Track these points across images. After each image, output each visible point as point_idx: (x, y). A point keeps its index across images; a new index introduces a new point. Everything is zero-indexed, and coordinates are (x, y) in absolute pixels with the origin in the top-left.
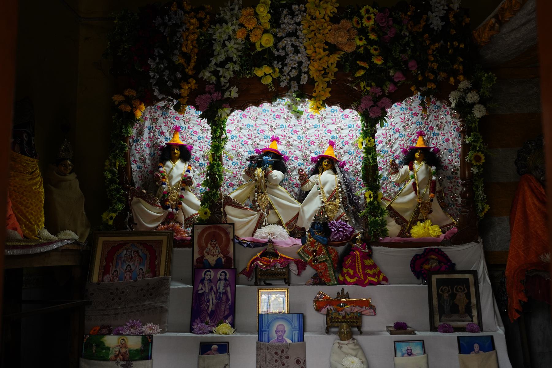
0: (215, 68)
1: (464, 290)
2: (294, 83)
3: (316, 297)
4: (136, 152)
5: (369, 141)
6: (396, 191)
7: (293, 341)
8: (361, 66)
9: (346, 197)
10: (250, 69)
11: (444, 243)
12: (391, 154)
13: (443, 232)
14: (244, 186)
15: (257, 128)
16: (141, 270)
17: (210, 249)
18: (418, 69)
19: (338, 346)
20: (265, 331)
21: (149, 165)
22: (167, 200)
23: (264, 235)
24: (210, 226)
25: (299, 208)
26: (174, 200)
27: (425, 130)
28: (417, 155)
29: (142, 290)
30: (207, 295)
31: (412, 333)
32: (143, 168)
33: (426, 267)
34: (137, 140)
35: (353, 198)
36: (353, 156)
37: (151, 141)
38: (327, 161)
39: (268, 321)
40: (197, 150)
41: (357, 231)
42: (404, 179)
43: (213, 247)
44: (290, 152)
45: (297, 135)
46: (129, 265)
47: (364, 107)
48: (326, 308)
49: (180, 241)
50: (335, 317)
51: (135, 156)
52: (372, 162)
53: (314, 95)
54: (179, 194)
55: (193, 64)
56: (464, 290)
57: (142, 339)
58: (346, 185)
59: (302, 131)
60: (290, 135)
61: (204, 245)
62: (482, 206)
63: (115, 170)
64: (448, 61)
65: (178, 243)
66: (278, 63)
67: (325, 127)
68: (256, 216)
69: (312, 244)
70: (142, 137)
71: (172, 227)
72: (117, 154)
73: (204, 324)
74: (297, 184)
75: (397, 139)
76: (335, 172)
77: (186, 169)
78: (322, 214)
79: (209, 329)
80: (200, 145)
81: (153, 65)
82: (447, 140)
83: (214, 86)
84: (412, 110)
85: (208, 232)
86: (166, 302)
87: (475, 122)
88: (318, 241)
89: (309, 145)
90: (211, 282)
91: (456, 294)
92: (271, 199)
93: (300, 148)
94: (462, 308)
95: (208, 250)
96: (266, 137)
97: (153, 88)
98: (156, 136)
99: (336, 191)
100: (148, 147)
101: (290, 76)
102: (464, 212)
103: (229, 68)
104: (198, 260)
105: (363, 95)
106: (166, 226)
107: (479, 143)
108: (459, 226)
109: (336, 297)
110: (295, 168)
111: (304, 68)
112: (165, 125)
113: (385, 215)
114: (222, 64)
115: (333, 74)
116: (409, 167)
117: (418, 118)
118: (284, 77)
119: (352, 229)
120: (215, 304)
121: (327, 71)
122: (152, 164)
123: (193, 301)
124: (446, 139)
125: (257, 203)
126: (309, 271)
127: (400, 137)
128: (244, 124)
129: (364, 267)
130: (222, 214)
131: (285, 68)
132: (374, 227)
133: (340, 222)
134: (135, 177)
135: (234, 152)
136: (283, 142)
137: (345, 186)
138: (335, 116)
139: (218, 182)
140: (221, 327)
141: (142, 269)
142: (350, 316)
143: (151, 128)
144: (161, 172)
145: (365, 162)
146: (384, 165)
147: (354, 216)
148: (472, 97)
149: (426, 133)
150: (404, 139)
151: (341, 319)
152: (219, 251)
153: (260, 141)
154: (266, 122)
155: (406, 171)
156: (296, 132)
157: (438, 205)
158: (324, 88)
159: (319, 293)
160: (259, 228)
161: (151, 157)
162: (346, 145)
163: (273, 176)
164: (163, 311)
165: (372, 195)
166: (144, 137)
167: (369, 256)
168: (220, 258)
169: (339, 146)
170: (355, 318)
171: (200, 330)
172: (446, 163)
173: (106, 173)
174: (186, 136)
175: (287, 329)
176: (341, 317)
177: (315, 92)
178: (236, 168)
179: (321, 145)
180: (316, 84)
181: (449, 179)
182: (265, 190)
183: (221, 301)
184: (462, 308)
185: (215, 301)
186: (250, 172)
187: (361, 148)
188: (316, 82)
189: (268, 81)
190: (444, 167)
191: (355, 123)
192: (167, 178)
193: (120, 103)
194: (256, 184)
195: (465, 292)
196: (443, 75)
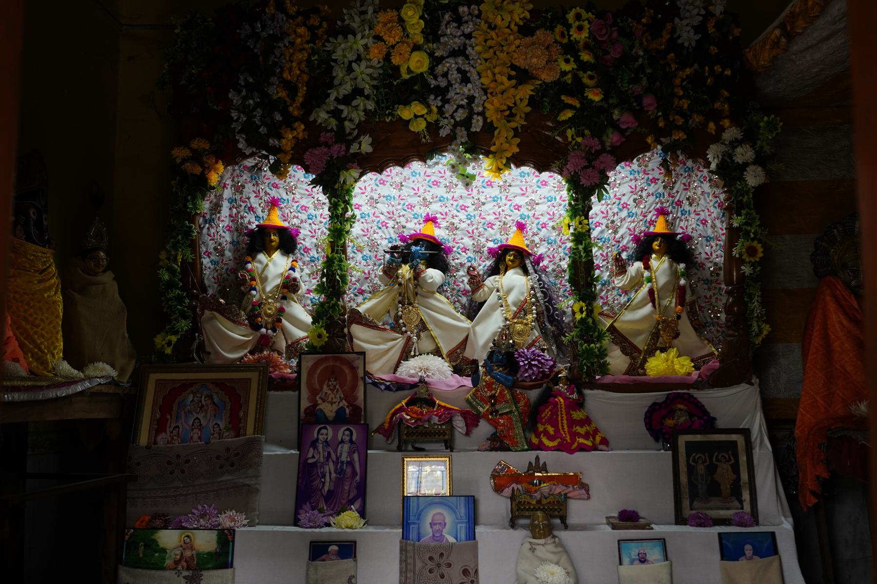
0: (335, 105)
4: (210, 238)
6: (622, 302)
9: (543, 311)
10: (391, 107)
11: (697, 385)
12: (614, 243)
13: (697, 368)
14: (382, 293)
15: (402, 202)
16: (216, 426)
17: (326, 393)
19: (530, 547)
20: (414, 523)
21: (230, 260)
22: (259, 315)
23: (412, 372)
24: (326, 357)
25: (469, 329)
26: (269, 316)
27: (669, 206)
28: (656, 245)
29: (218, 457)
33: (670, 422)
34: (210, 220)
35: (553, 312)
36: (555, 247)
37: (232, 221)
38: (513, 254)
39: (418, 508)
41: (560, 366)
42: (636, 283)
43: (330, 389)
44: (454, 239)
45: (466, 213)
46: (197, 418)
48: (511, 488)
50: (525, 501)
51: (208, 245)
52: (585, 256)
53: (493, 149)
54: (278, 305)
58: (542, 292)
59: (474, 207)
60: (455, 212)
61: (318, 387)
62: (759, 326)
63: (176, 266)
64: (706, 96)
65: (275, 383)
66: (435, 99)
67: (510, 200)
68: (400, 341)
69: (489, 386)
70: (218, 215)
71: (266, 358)
72: (178, 242)
73: (316, 512)
74: (464, 290)
75: (624, 219)
76: (526, 272)
77: (289, 266)
78: (504, 338)
80: (312, 228)
82: (704, 222)
84: (648, 174)
85: (324, 366)
86: (256, 476)
88: (498, 380)
89: (485, 229)
90: (329, 445)
91: (717, 466)
92: (424, 313)
93: (469, 233)
94: (726, 488)
95: (324, 394)
96: (416, 216)
97: (237, 138)
98: (242, 213)
99: (526, 302)
100: (229, 230)
101: (455, 119)
102: (730, 336)
103: (358, 106)
104: (308, 411)
105: (571, 150)
106: (256, 356)
107: (754, 226)
110: (462, 265)
111: (478, 106)
112: (256, 197)
113: (604, 340)
114: (347, 100)
115: (523, 116)
116: (643, 264)
117: (657, 186)
118: (446, 121)
121: (514, 111)
122: (235, 258)
123: (300, 475)
124: (702, 221)
125: (401, 321)
126: (484, 429)
127: (629, 216)
128: (382, 195)
129: (572, 422)
130: (347, 338)
131: (447, 106)
132: (587, 359)
133: (534, 351)
134: (207, 279)
135: (366, 238)
139: (340, 286)
140: (343, 516)
142: (548, 500)
143: (232, 200)
144: (248, 271)
146: (604, 260)
148: (743, 154)
149: (669, 210)
150: (636, 219)
152: (340, 397)
153: (407, 221)
154: (417, 192)
155: (638, 270)
156: (464, 208)
158: (509, 138)
159: (499, 464)
160: (404, 360)
163: (428, 277)
164: (252, 491)
165: (584, 309)
166: (222, 215)
167: (579, 404)
168: (342, 407)
169: (532, 231)
171: (309, 521)
172: (701, 258)
173: (160, 272)
174: (289, 214)
178: (369, 265)
179: (504, 228)
182: (415, 300)
183: (344, 476)
184: (726, 488)
185: (334, 475)
186: (390, 271)
187: (568, 233)
188: (496, 128)
189: (419, 126)
190: (699, 264)
192: (258, 280)
193: (184, 161)
194: (400, 290)
196: (697, 119)
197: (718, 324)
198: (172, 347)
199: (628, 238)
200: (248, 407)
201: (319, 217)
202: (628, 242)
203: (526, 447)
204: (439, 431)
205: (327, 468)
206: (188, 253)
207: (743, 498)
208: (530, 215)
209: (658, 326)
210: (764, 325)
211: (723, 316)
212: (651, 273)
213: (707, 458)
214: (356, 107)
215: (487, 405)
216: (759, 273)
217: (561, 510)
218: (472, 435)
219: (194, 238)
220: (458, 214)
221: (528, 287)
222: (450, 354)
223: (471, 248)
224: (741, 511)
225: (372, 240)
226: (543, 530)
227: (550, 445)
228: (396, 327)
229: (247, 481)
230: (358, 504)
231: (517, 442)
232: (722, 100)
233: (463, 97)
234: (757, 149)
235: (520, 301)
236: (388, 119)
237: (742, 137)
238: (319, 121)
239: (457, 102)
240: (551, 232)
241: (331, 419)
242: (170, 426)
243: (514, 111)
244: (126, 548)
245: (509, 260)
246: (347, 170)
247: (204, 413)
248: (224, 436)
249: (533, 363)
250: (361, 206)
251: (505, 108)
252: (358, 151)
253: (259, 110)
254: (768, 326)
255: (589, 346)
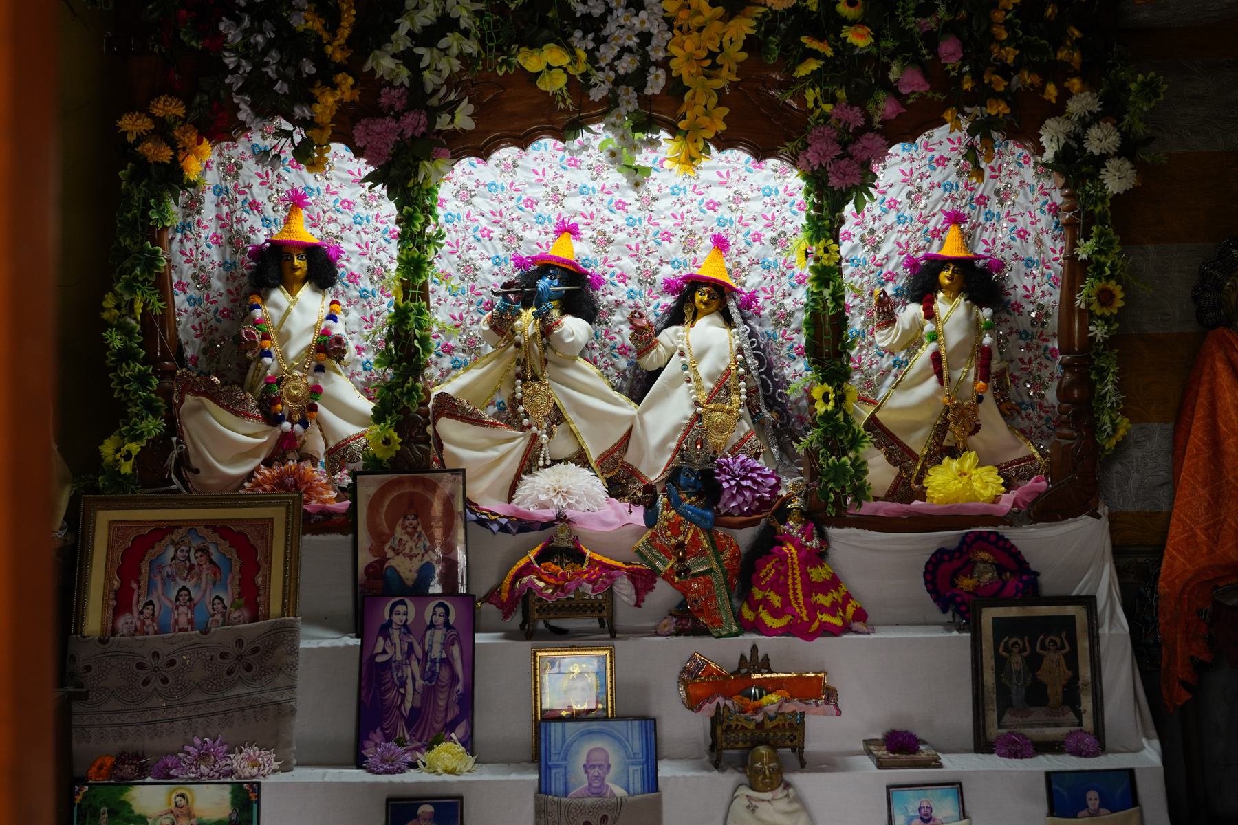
0: (409, 44)
1: (1063, 647)
2: (627, 90)
3: (685, 668)
4: (185, 258)
5: (826, 250)
6: (885, 366)
7: (631, 790)
8: (811, 49)
9: (757, 386)
10: (505, 48)
11: (1010, 519)
12: (873, 267)
13: (1008, 485)
14: (486, 360)
15: (516, 195)
16: (217, 601)
17: (401, 540)
18: (964, 61)
19: (748, 803)
20: (558, 766)
21: (221, 295)
22: (278, 400)
23: (543, 497)
24: (398, 479)
25: (633, 417)
26: (295, 400)
27: (966, 205)
28: (944, 277)
29: (223, 656)
30: (398, 669)
31: (933, 763)
32: (205, 304)
33: (966, 583)
34: (184, 226)
35: (774, 391)
36: (775, 274)
37: (222, 227)
38: (708, 292)
39: (564, 741)
40: (351, 252)
41: (788, 482)
42: (911, 343)
43: (408, 533)
44: (606, 260)
45: (626, 216)
46: (184, 588)
47: (815, 164)
48: (715, 703)
49: (321, 517)
50: (737, 725)
51: (181, 272)
52: (834, 308)
53: (681, 125)
54: (310, 380)
55: (345, 32)
56: (1063, 647)
57: (233, 792)
58: (756, 356)
59: (638, 204)
60: (607, 213)
61: (386, 530)
62: (1112, 421)
63: (133, 322)
64: (1044, 41)
65: (312, 521)
66: (584, 37)
67: (701, 193)
68: (520, 443)
69: (674, 527)
70: (197, 217)
71: (293, 474)
72: (136, 279)
73: (392, 745)
74: (623, 346)
75: (892, 227)
76: (728, 321)
77: (326, 312)
78: (699, 447)
79: (409, 758)
80: (361, 239)
81: (235, 36)
82: (1023, 234)
83: (403, 90)
84: (932, 150)
85: (395, 494)
86: (291, 687)
87: (1102, 200)
88: (688, 518)
89: (658, 243)
90: (409, 632)
91: (1042, 657)
92: (559, 393)
93: (631, 249)
94: (1055, 692)
95: (396, 542)
96: (541, 219)
97: (236, 101)
98: (238, 214)
99: (730, 373)
100: (216, 243)
101: (616, 72)
102: (1066, 437)
103: (448, 48)
104: (371, 570)
105: (812, 124)
106: (276, 470)
107: (1111, 255)
108: (1054, 471)
109: (735, 668)
110: (618, 304)
111: (656, 49)
112: (262, 184)
113: (863, 447)
114: (430, 36)
115: (734, 67)
116: (924, 310)
117: (947, 171)
118: (601, 75)
119: (773, 481)
120: (420, 690)
121: (719, 60)
122: (229, 291)
123: (363, 684)
124: (1019, 232)
125: (521, 409)
126: (663, 594)
127: (899, 222)
128: (482, 181)
129: (811, 588)
130: (431, 442)
131: (602, 48)
132: (834, 480)
133: (743, 462)
134: (183, 330)
135: (454, 258)
136: (586, 233)
138: (728, 162)
139: (419, 357)
140: (439, 753)
141: (221, 599)
142: (775, 722)
143: (221, 190)
144: (256, 323)
145: (812, 304)
146: (856, 297)
147: (778, 443)
148: (1100, 139)
149: (966, 213)
150: (910, 228)
151: (751, 730)
152: (424, 546)
153: (525, 228)
154: (541, 177)
155: (914, 319)
156: (622, 206)
157: (995, 409)
158: (710, 107)
159: (692, 658)
160: (525, 474)
161: (224, 272)
162: (757, 243)
163: (565, 334)
164: (284, 712)
165: (831, 396)
166: (204, 216)
167: (819, 556)
168: (428, 563)
169: (737, 246)
170: (787, 727)
171: (384, 761)
172: (1016, 296)
173: (107, 335)
174: (321, 214)
175: (614, 760)
176: (752, 726)
177: (684, 117)
178: (461, 304)
179: (690, 244)
180: (688, 96)
181: (1025, 339)
182: (543, 372)
183: (437, 683)
184: (1055, 692)
185: (420, 682)
186: (501, 325)
187: (804, 268)
188: (688, 88)
189: (555, 83)
190: (1013, 305)
191: (780, 184)
192: (274, 339)
193: (140, 140)
194: (518, 356)
195: (1063, 652)
196: (1027, 78)
197: (1041, 406)
198: (132, 461)
199: (896, 259)
200: (270, 568)
201: (373, 221)
202: (897, 267)
203: (735, 628)
204: (593, 605)
205: (408, 672)
206: (154, 299)
207: (1082, 708)
208: (734, 219)
209: (947, 414)
210: (1120, 418)
211: (1051, 396)
212: (937, 325)
213: (1027, 645)
214: (445, 51)
215: (670, 559)
216: (1115, 333)
217: (795, 738)
218: (643, 604)
219: (162, 271)
220: (612, 216)
221: (732, 348)
222: (602, 460)
223: (634, 275)
224: (1079, 728)
225: (466, 261)
226: (770, 778)
227: (775, 626)
229: (276, 697)
230: (461, 730)
231: (721, 621)
232: (1069, 43)
233: (630, 33)
234: (1123, 129)
235: (719, 371)
236: (501, 70)
237: (1100, 109)
238: (380, 72)
239: (621, 42)
240: (769, 249)
241: (410, 583)
242: (138, 602)
243: (719, 60)
244: (78, 817)
245: (701, 301)
246: (432, 159)
247: (195, 579)
248: (232, 618)
249: (744, 483)
250: (446, 201)
251: (705, 54)
252: (450, 127)
253: (274, 53)
254: (1126, 420)
255: (839, 460)
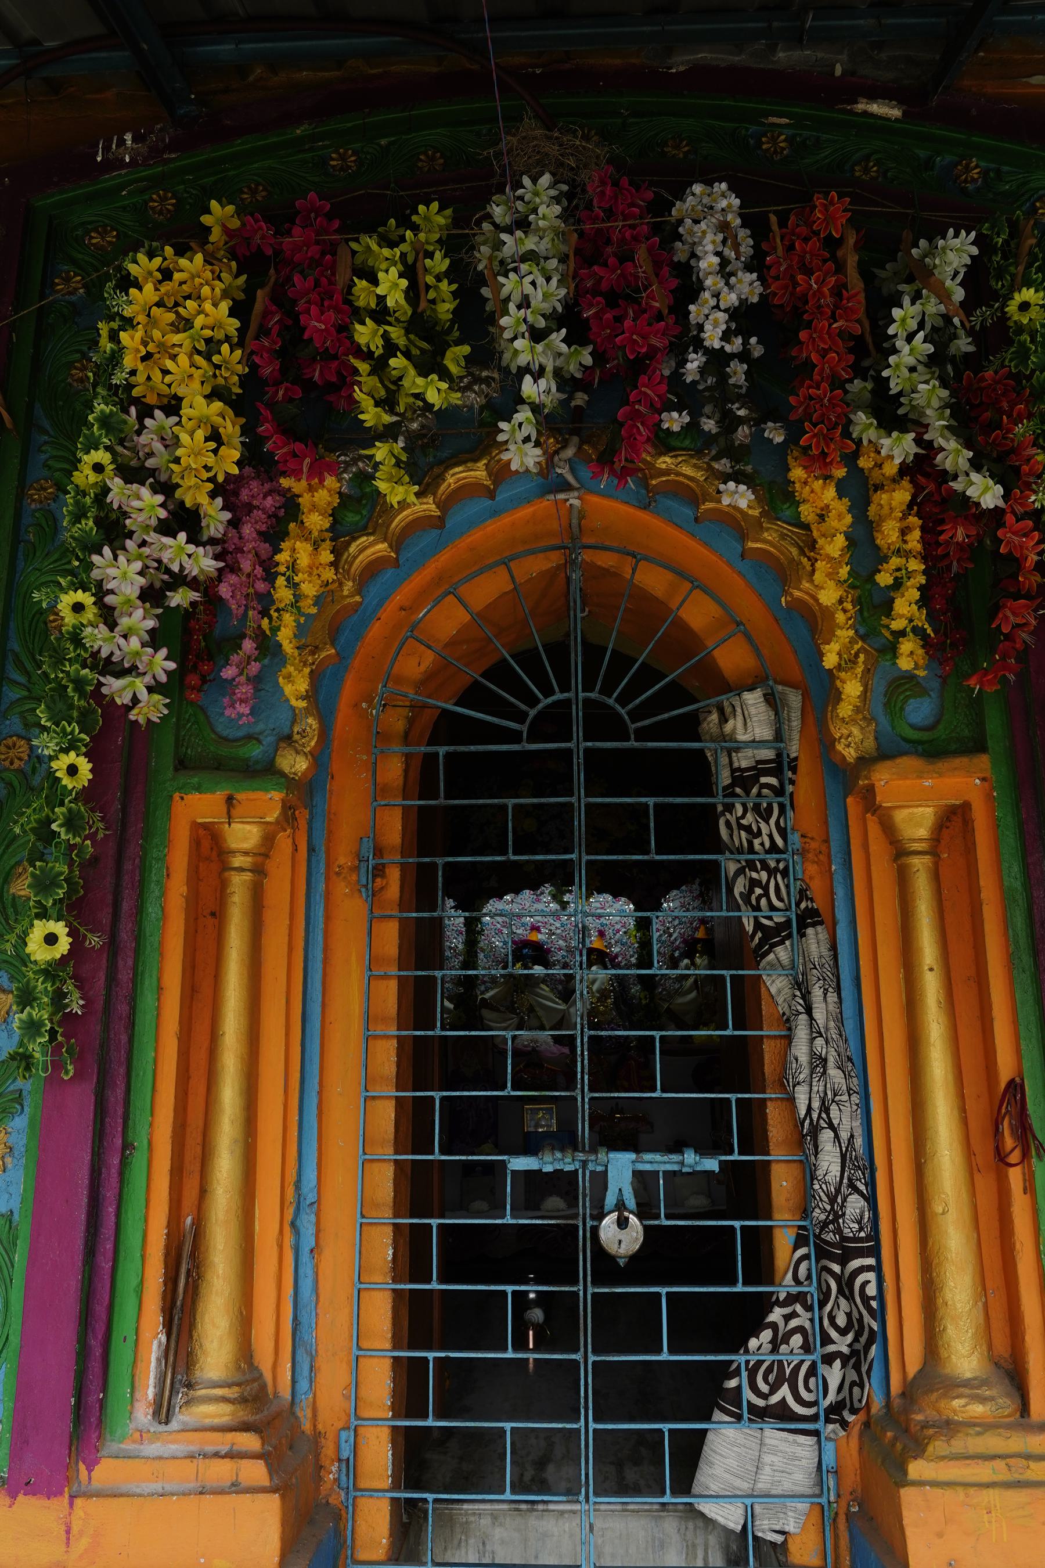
110: (559, 961)
137: (269, 498)
228: (512, 1009)
